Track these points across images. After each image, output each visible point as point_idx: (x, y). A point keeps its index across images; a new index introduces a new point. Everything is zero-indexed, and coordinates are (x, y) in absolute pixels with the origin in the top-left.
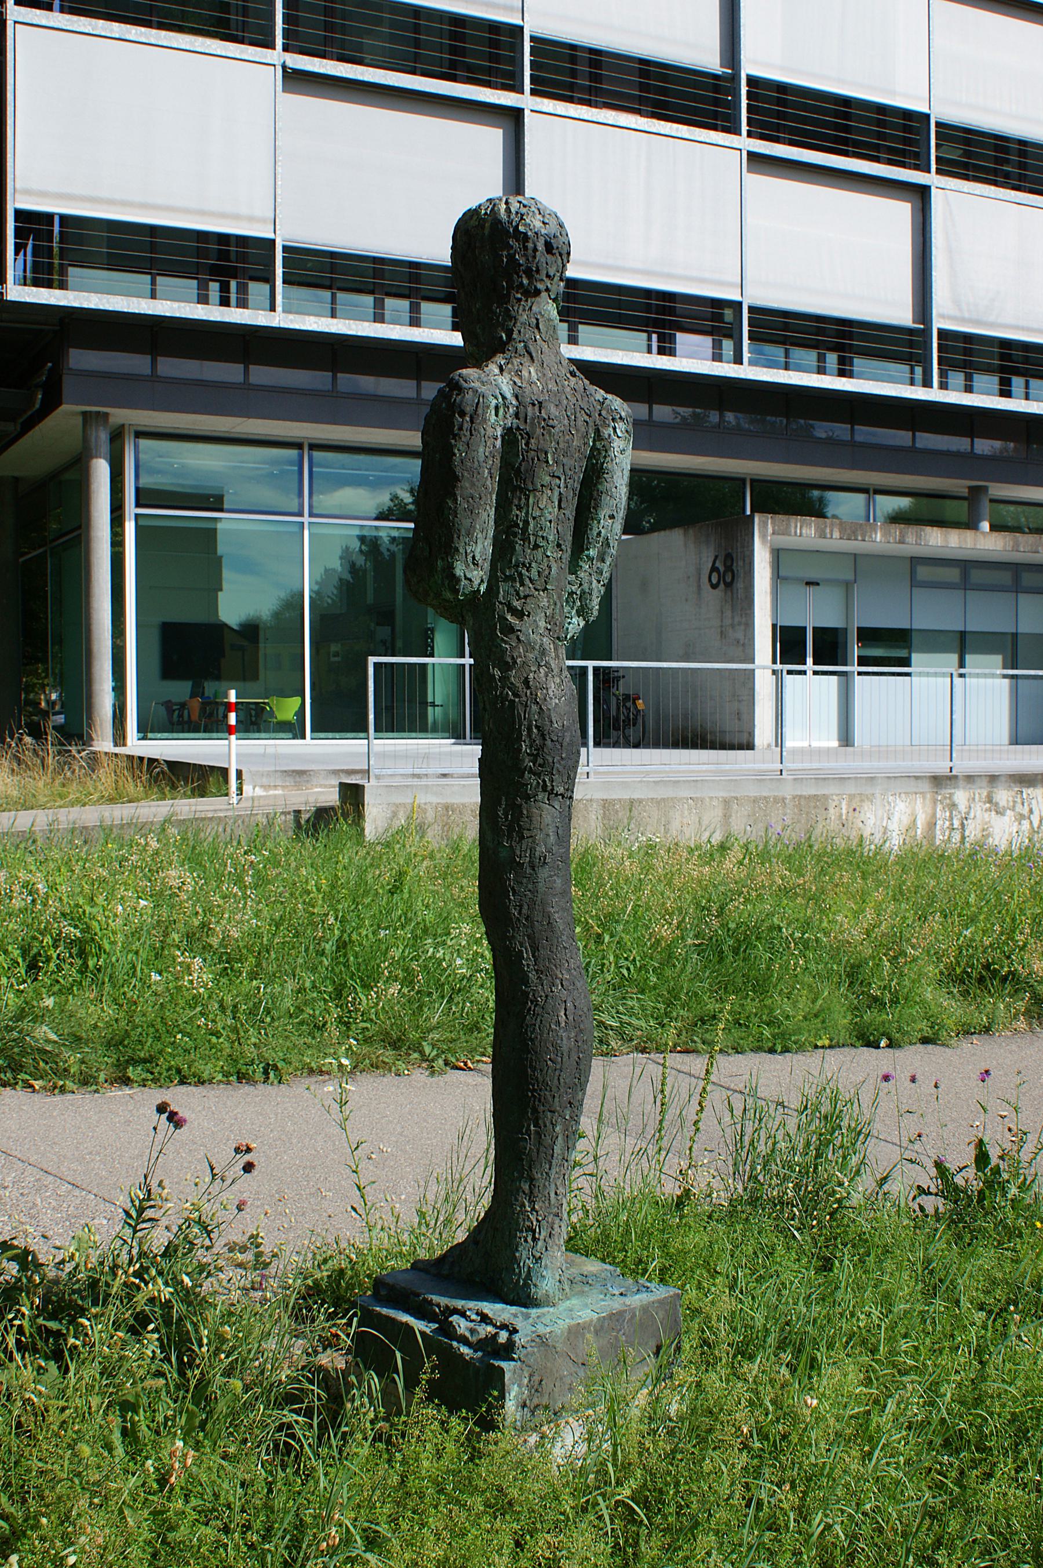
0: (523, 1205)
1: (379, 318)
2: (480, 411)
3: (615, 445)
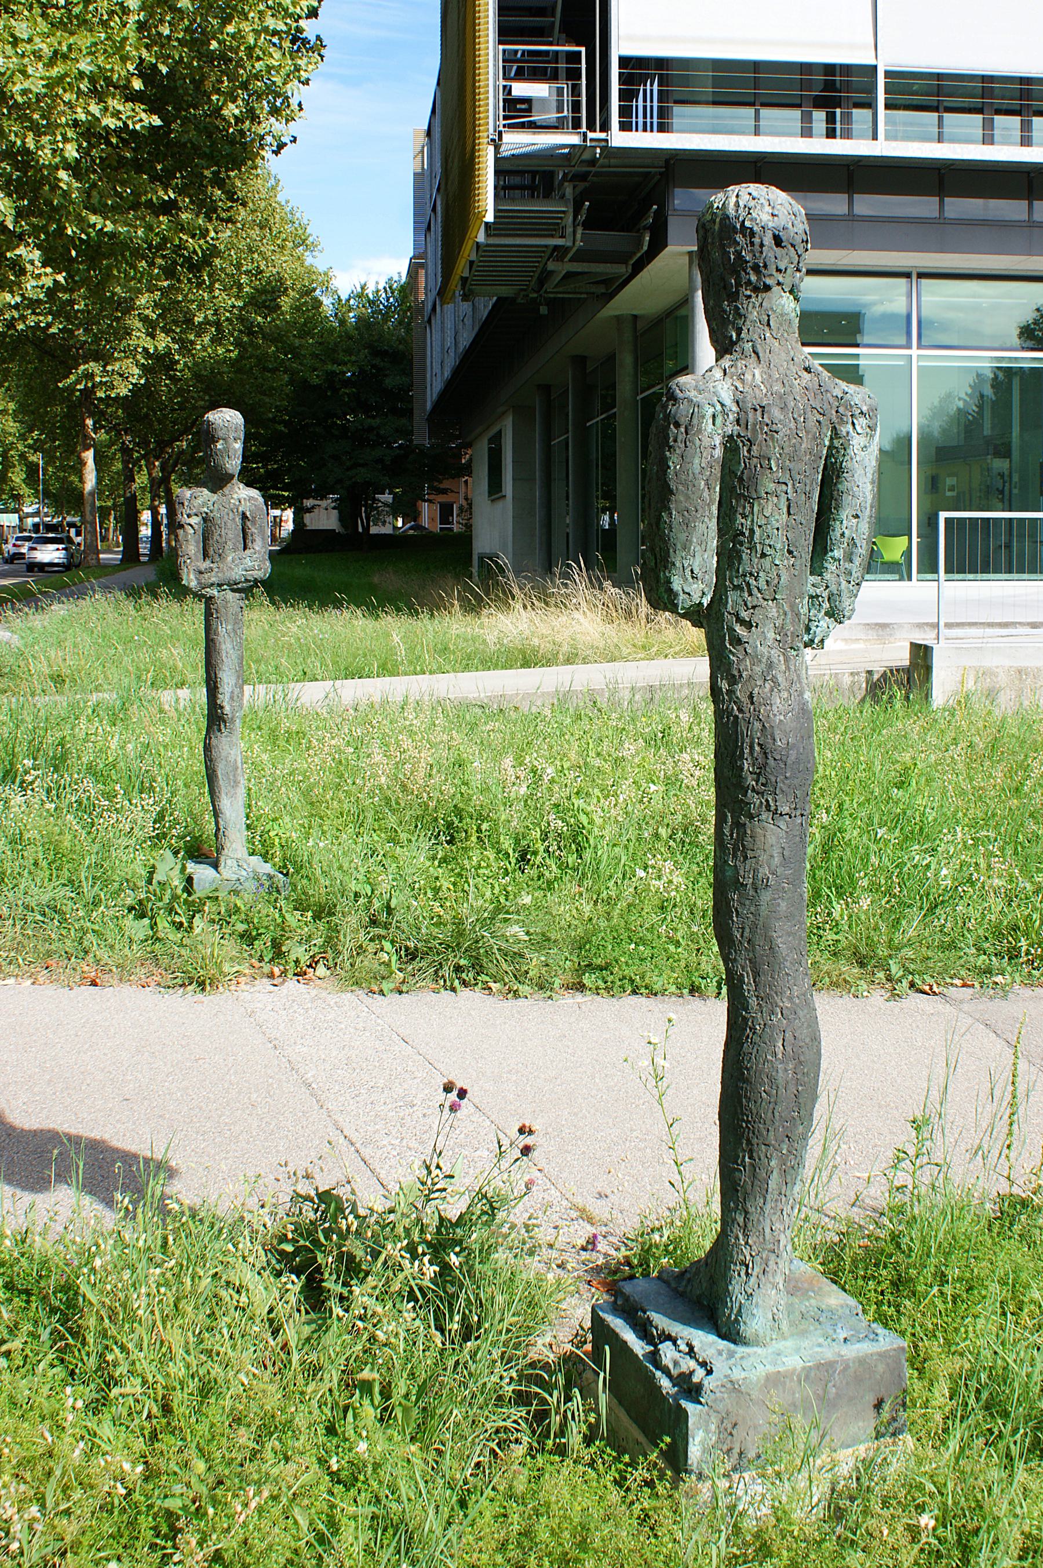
0: (737, 1238)
1: (988, 139)
2: (695, 421)
3: (854, 442)
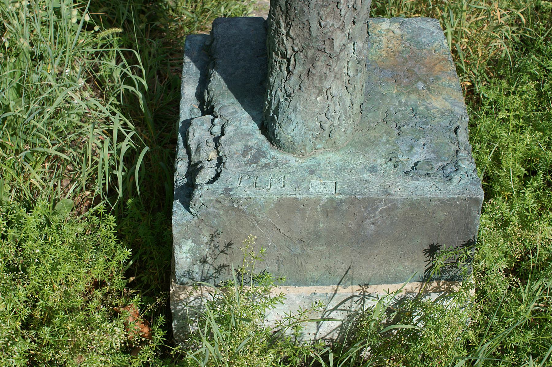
0: (278, 24)
